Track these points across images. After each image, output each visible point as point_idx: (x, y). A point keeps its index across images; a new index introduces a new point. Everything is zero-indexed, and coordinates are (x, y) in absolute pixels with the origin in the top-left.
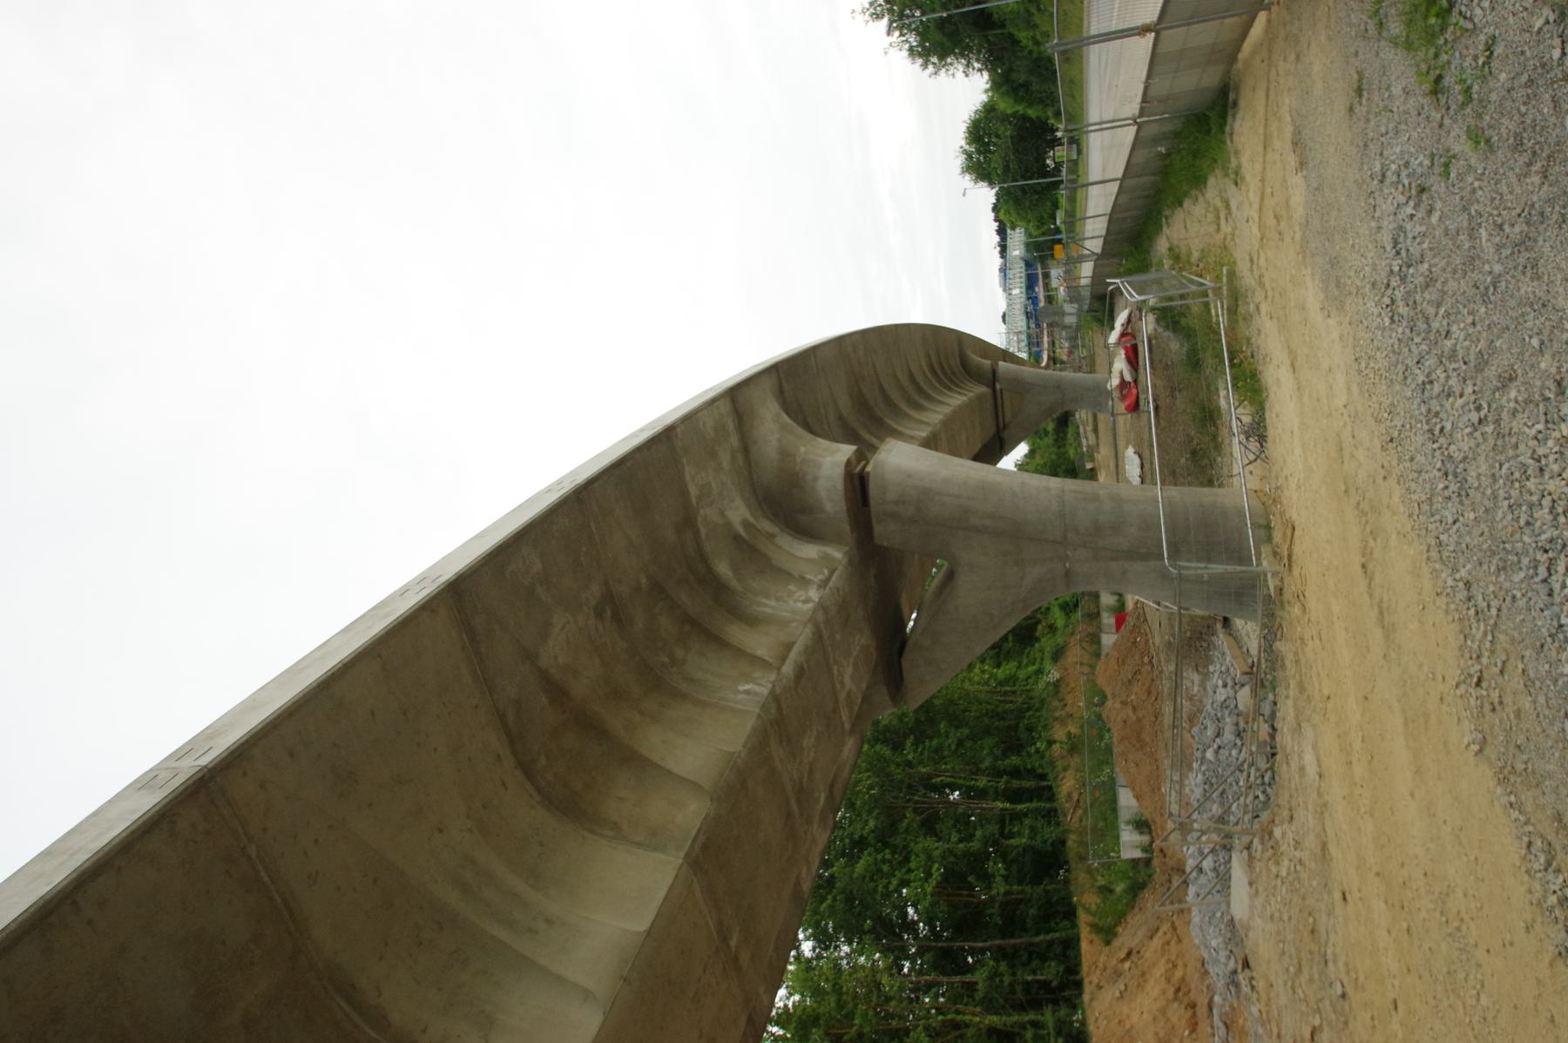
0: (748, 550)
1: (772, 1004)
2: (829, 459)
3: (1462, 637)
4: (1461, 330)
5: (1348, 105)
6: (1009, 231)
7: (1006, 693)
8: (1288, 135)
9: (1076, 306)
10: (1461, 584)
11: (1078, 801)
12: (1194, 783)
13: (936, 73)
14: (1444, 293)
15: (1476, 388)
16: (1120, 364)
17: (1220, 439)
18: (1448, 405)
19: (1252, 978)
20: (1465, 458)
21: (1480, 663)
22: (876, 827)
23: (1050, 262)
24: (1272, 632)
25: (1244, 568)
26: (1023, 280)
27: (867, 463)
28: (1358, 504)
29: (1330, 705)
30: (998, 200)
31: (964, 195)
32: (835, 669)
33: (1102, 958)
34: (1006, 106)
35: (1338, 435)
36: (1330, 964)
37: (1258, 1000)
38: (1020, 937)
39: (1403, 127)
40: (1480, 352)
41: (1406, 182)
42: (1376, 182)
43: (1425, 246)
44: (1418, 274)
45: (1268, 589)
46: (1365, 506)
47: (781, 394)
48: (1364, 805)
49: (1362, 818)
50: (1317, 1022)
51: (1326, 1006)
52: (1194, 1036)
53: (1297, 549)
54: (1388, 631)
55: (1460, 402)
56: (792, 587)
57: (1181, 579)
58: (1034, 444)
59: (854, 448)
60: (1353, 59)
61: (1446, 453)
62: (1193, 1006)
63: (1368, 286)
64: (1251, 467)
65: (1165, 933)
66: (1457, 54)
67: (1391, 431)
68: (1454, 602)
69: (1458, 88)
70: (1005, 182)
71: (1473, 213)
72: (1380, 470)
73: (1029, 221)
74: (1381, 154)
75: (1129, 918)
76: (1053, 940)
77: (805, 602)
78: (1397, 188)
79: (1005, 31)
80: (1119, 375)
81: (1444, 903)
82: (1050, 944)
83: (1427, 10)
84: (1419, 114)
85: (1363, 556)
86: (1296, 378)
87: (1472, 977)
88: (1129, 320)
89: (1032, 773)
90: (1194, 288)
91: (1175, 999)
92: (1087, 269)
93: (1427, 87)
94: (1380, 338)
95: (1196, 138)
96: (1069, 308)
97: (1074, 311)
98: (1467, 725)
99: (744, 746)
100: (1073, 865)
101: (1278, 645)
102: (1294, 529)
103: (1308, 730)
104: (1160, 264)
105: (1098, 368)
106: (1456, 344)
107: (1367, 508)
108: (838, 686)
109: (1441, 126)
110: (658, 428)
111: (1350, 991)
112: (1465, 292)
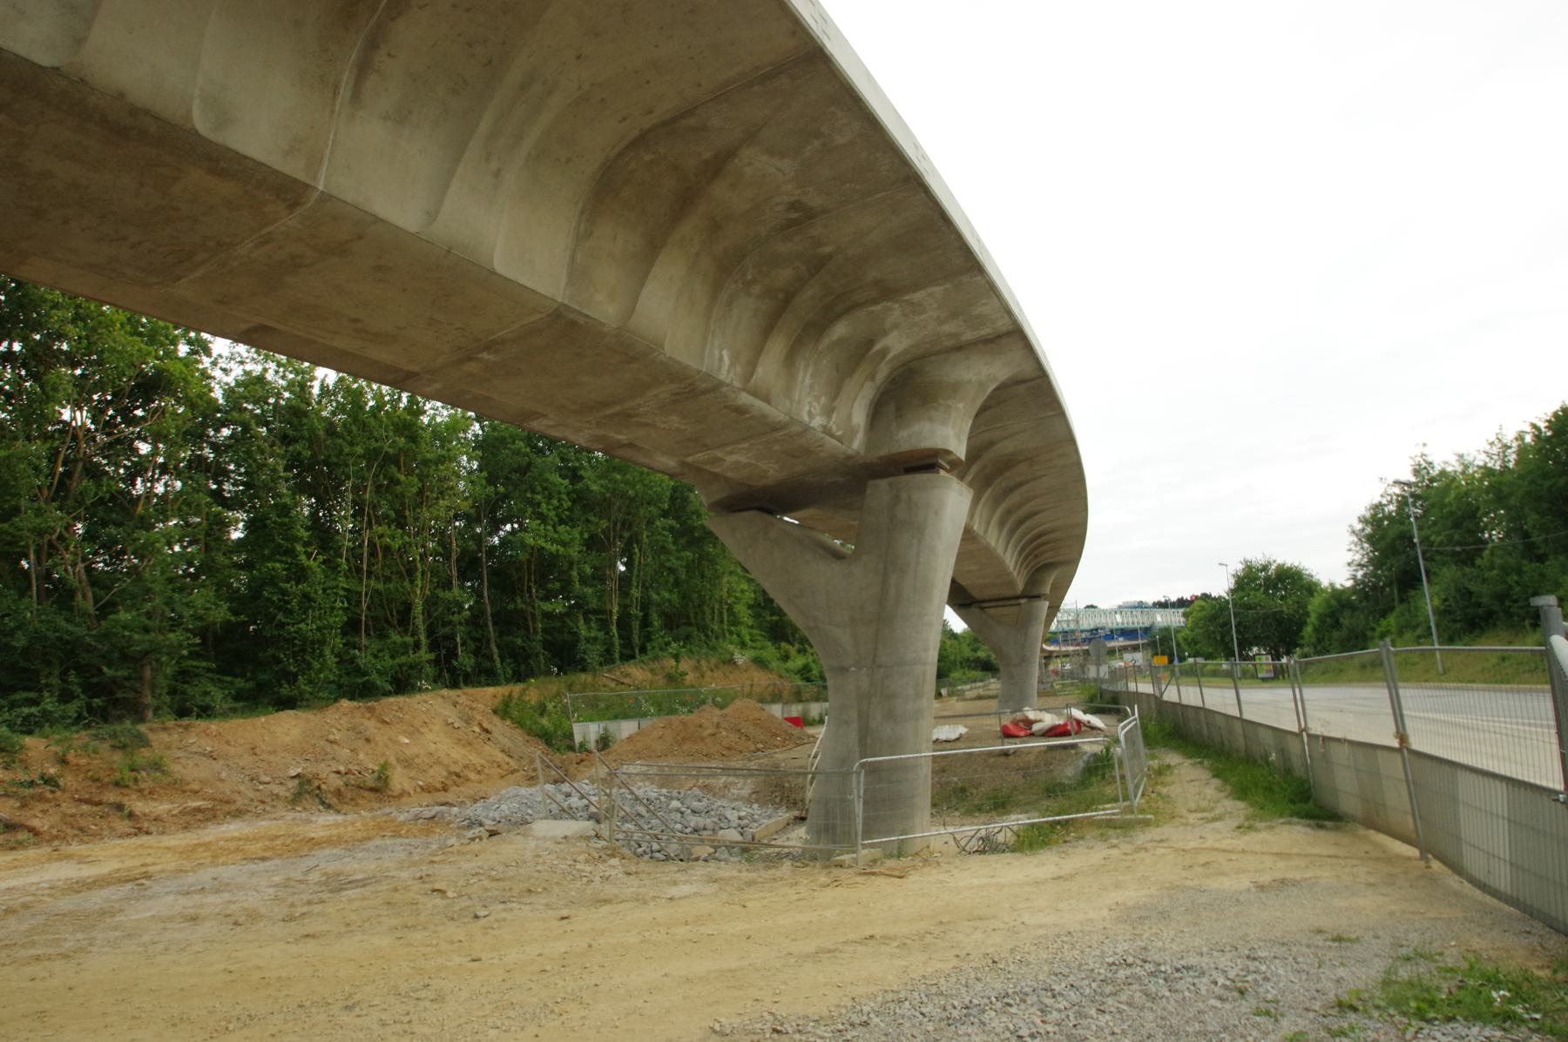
0: (860, 352)
1: (428, 398)
2: (952, 433)
3: (816, 1018)
4: (1107, 1023)
5: (1324, 929)
6: (1181, 610)
7: (721, 613)
8: (1290, 875)
9: (1107, 677)
10: (865, 1018)
11: (623, 683)
12: (648, 790)
13: (1353, 532)
14: (1142, 1009)
15: (1051, 1034)
16: (1049, 720)
17: (977, 814)
18: (1033, 1010)
19: (481, 839)
20: (984, 1024)
21: (794, 1032)
22: (592, 491)
23: (1150, 652)
24: (804, 858)
25: (860, 833)
26: (1131, 626)
27: (948, 471)
28: (930, 933)
29: (737, 908)
30: (1215, 599)
31: (1220, 564)
32: (745, 445)
33: (481, 707)
34: (1315, 605)
35: (995, 916)
36: (502, 906)
37: (462, 844)
38: (494, 631)
39: (1304, 977)
40: (1087, 1038)
41: (1249, 978)
42: (1247, 952)
43: (1187, 993)
44: (1158, 986)
45: (839, 855)
46: (929, 939)
47: (1016, 382)
48: (651, 935)
49: (639, 933)
50: (450, 894)
51: (465, 903)
52: (419, 790)
53: (881, 880)
54: (816, 956)
55: (1038, 1021)
56: (823, 399)
57: (845, 776)
58: (964, 638)
59: (963, 457)
60: (1371, 933)
61: (987, 1008)
62: (445, 789)
63: (1143, 944)
64: (952, 842)
65: (508, 764)
66: (1379, 1025)
67: (1003, 962)
68: (848, 1012)
69: (1346, 1025)
70: (1235, 605)
71: (1222, 1035)
72: (965, 952)
73: (1192, 631)
74: (1275, 957)
75: (519, 731)
76: (494, 661)
77: (810, 413)
78: (1242, 970)
79: (1396, 603)
80: (1038, 718)
81: (573, 1000)
82: (490, 658)
83: (1424, 1000)
84: (1317, 991)
85: (881, 937)
86: (1046, 880)
87: (512, 1022)
88: (1093, 728)
89: (648, 638)
90: (1131, 787)
91: (450, 773)
92: (1146, 688)
93: (1345, 998)
94: (1093, 953)
95: (1285, 790)
96: (1104, 671)
97: (1101, 675)
98: (736, 1021)
99: (670, 358)
100: (563, 678)
101: (787, 863)
102: (900, 877)
103: (710, 889)
104: (1153, 757)
105: (1043, 699)
106: (1092, 1018)
107: (927, 941)
108: (728, 449)
109: (1307, 1010)
110: (982, 257)
111: (482, 922)
112: (1143, 1026)
